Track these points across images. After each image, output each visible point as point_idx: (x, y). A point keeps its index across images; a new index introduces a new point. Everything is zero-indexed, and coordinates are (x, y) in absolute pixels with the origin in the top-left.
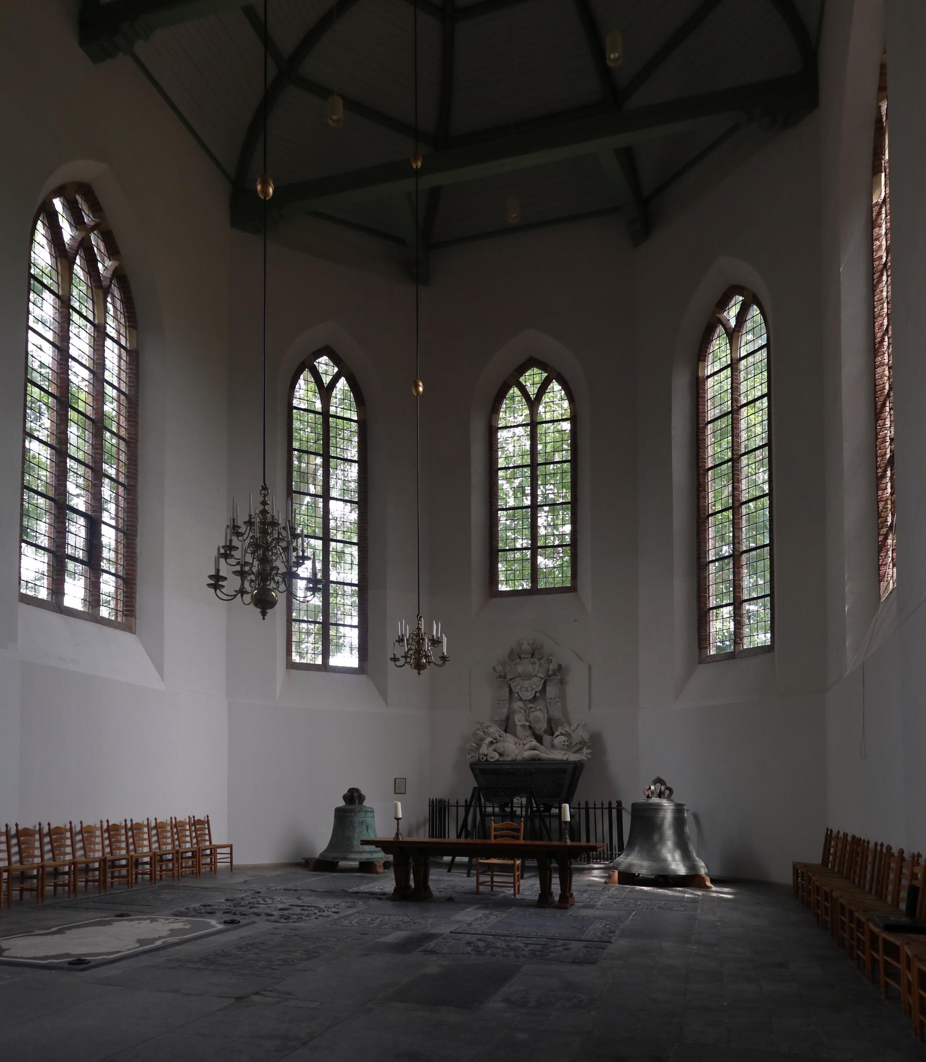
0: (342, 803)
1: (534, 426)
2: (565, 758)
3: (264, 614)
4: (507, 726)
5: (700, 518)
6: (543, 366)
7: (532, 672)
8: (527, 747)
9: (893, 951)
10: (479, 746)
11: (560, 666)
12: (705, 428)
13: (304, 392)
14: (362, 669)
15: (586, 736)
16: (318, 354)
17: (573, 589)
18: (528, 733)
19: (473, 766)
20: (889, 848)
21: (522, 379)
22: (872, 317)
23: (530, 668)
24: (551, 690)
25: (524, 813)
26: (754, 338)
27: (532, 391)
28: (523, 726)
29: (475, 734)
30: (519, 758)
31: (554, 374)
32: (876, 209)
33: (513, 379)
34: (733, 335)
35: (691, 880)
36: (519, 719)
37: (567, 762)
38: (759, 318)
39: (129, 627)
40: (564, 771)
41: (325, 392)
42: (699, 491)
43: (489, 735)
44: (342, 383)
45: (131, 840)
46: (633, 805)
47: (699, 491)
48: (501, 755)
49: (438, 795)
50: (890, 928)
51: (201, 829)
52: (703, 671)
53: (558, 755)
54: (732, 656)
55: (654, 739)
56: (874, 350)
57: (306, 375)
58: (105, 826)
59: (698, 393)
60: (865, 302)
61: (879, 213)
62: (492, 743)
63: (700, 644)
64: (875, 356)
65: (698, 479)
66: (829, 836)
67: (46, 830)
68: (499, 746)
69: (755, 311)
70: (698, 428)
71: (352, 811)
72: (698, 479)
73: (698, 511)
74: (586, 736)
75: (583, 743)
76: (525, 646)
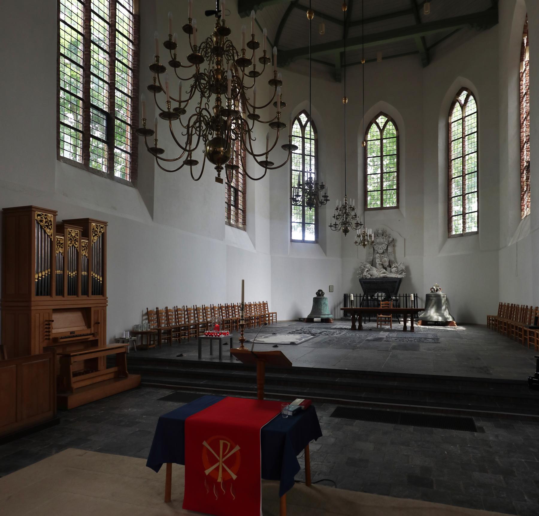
0: (316, 296)
1: (380, 139)
2: (396, 277)
3: (346, 235)
4: (373, 264)
5: (449, 180)
6: (386, 115)
7: (382, 243)
8: (382, 272)
9: (531, 333)
10: (362, 273)
11: (393, 239)
12: (451, 143)
13: (296, 128)
14: (316, 242)
15: (404, 268)
16: (300, 114)
17: (397, 207)
18: (381, 267)
19: (360, 280)
20: (527, 306)
21: (377, 120)
22: (520, 114)
23: (382, 240)
24: (390, 249)
25: (380, 299)
26: (472, 106)
27: (381, 126)
28: (380, 264)
29: (360, 267)
30: (378, 277)
31: (390, 119)
32: (521, 74)
33: (374, 121)
34: (463, 107)
35: (445, 323)
36: (378, 261)
37: (397, 278)
38: (474, 101)
39: (244, 229)
40: (396, 282)
41: (303, 128)
42: (448, 169)
43: (366, 268)
44: (309, 124)
45: (196, 315)
46: (427, 295)
47: (448, 169)
48: (371, 276)
49: (345, 293)
50: (531, 328)
51: (180, 314)
52: (450, 241)
53: (393, 275)
54: (461, 235)
55: (429, 268)
56: (520, 126)
57: (296, 122)
58: (186, 309)
59: (448, 129)
60: (518, 107)
61: (522, 76)
62: (368, 271)
63: (448, 230)
64: (521, 129)
65: (448, 164)
66: (501, 306)
67: (186, 309)
68: (371, 272)
69: (471, 98)
70: (448, 143)
71: (321, 299)
72: (448, 164)
73: (448, 177)
74: (404, 268)
75: (403, 270)
76: (380, 232)
